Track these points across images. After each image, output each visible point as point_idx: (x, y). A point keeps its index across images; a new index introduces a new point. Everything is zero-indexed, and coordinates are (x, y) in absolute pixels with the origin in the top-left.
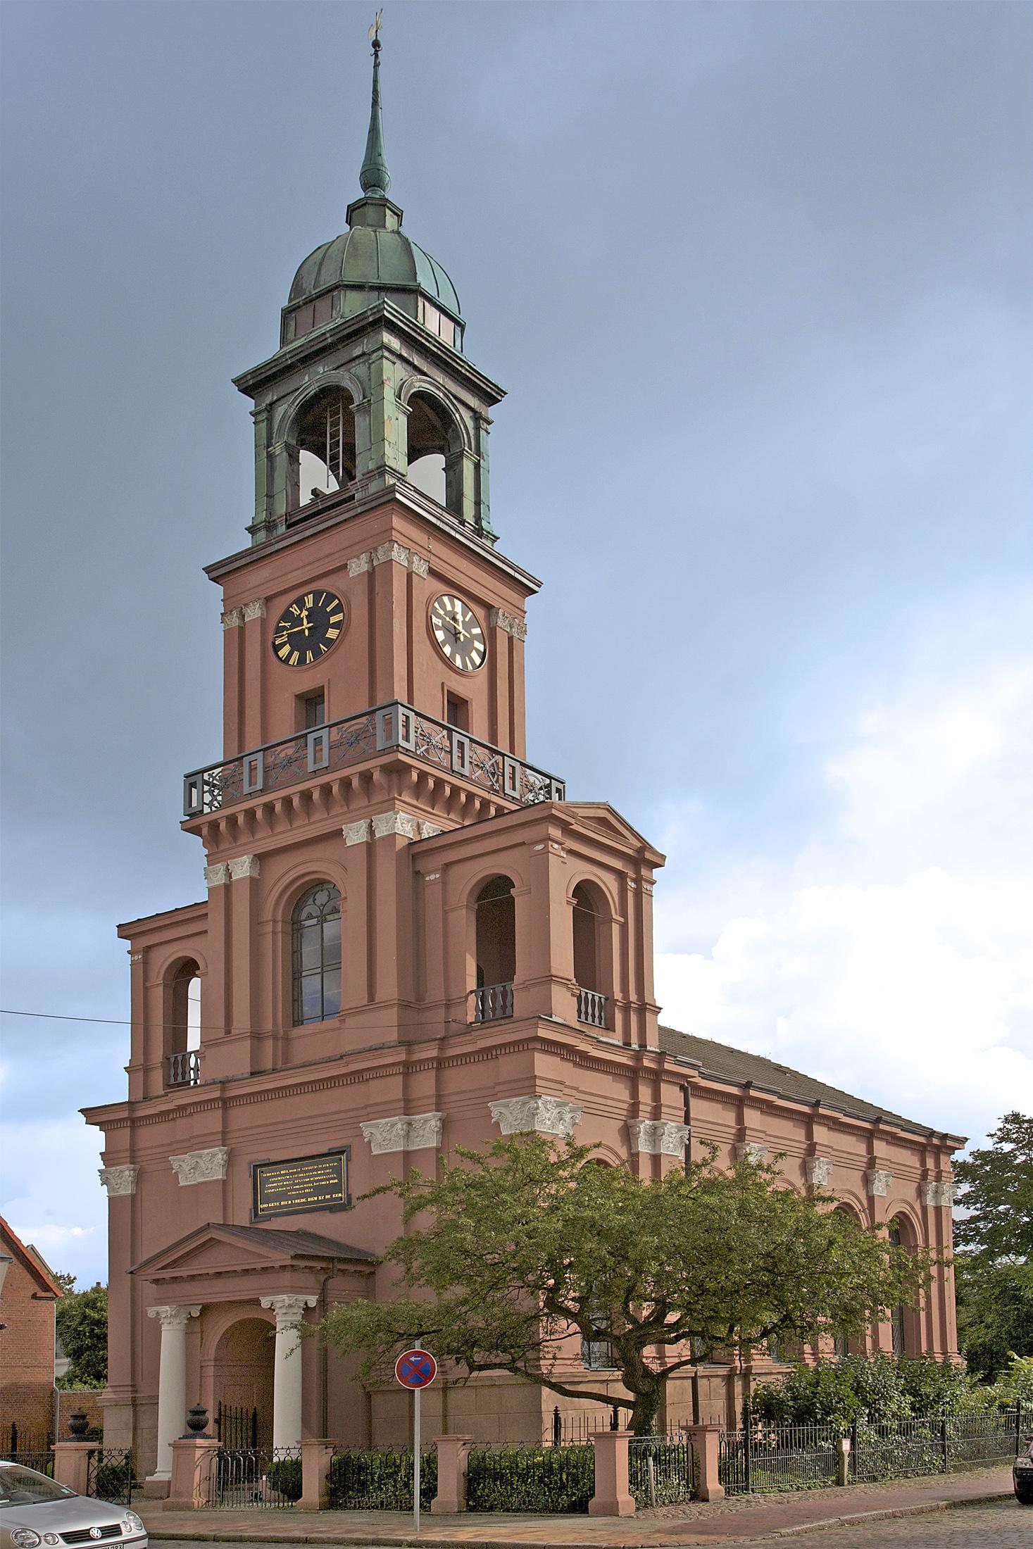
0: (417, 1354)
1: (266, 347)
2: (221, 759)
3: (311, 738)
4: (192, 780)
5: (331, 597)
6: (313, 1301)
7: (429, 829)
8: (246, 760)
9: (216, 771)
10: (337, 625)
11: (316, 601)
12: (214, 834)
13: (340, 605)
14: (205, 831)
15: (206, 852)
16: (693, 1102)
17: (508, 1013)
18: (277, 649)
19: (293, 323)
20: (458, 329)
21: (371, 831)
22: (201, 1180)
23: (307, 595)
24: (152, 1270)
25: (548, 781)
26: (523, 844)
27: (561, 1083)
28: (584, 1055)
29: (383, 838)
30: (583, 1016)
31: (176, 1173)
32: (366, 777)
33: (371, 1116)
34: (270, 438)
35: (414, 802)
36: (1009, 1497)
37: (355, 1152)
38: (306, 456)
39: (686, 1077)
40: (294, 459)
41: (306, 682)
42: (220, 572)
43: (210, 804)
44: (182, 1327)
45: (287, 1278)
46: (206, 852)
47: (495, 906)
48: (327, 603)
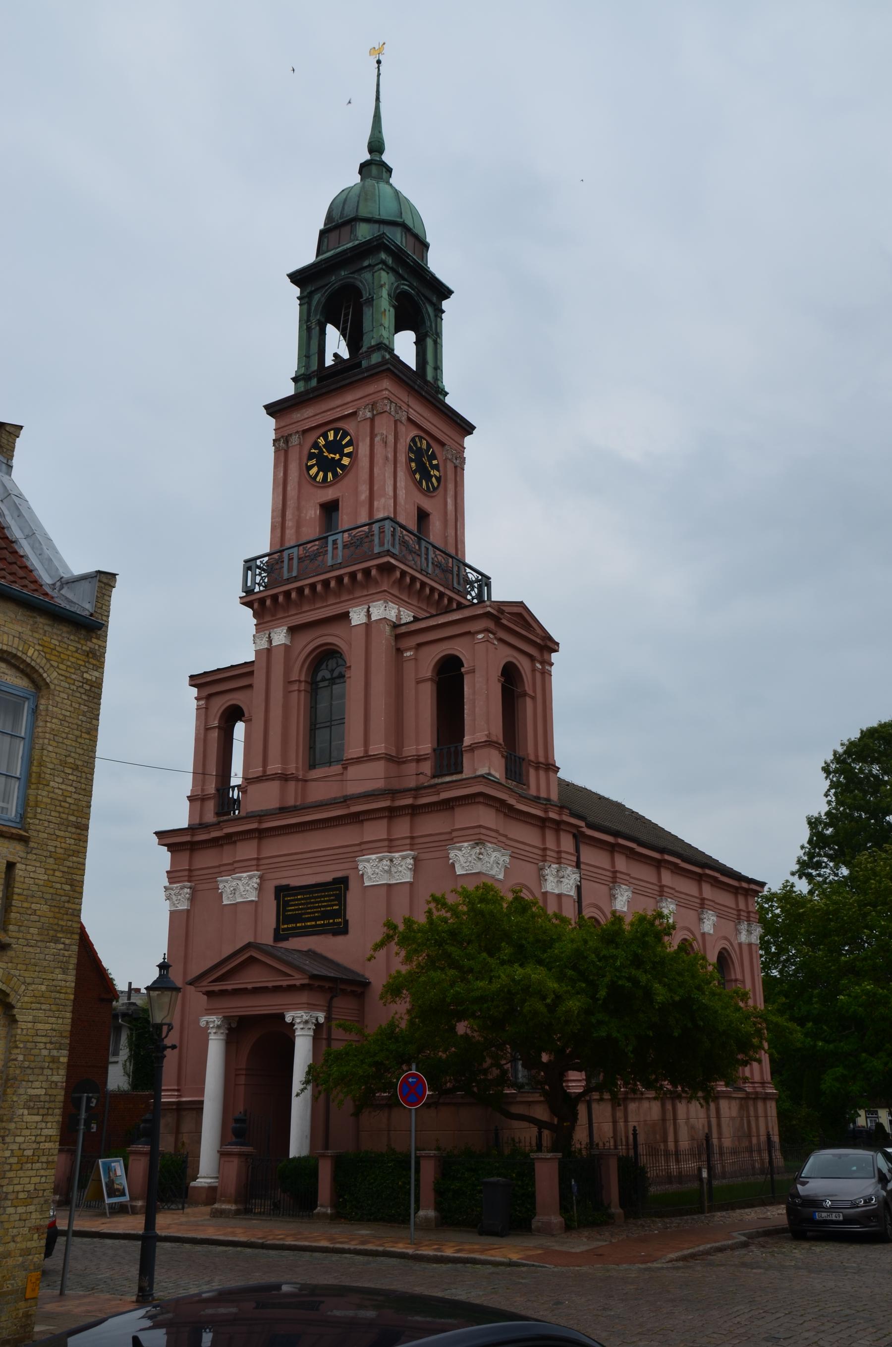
0: (413, 1076)
1: (307, 256)
3: (331, 539)
4: (249, 564)
5: (346, 434)
8: (286, 554)
10: (349, 455)
11: (335, 436)
12: (262, 606)
13: (351, 440)
14: (256, 605)
15: (255, 621)
18: (309, 468)
19: (326, 240)
21: (369, 615)
23: (330, 430)
24: (205, 983)
26: (469, 633)
28: (511, 807)
31: (222, 893)
32: (367, 572)
33: (364, 852)
35: (398, 595)
36: (783, 1231)
37: (352, 884)
41: (329, 495)
42: (273, 409)
43: (259, 584)
45: (304, 998)
47: (449, 678)
48: (343, 438)
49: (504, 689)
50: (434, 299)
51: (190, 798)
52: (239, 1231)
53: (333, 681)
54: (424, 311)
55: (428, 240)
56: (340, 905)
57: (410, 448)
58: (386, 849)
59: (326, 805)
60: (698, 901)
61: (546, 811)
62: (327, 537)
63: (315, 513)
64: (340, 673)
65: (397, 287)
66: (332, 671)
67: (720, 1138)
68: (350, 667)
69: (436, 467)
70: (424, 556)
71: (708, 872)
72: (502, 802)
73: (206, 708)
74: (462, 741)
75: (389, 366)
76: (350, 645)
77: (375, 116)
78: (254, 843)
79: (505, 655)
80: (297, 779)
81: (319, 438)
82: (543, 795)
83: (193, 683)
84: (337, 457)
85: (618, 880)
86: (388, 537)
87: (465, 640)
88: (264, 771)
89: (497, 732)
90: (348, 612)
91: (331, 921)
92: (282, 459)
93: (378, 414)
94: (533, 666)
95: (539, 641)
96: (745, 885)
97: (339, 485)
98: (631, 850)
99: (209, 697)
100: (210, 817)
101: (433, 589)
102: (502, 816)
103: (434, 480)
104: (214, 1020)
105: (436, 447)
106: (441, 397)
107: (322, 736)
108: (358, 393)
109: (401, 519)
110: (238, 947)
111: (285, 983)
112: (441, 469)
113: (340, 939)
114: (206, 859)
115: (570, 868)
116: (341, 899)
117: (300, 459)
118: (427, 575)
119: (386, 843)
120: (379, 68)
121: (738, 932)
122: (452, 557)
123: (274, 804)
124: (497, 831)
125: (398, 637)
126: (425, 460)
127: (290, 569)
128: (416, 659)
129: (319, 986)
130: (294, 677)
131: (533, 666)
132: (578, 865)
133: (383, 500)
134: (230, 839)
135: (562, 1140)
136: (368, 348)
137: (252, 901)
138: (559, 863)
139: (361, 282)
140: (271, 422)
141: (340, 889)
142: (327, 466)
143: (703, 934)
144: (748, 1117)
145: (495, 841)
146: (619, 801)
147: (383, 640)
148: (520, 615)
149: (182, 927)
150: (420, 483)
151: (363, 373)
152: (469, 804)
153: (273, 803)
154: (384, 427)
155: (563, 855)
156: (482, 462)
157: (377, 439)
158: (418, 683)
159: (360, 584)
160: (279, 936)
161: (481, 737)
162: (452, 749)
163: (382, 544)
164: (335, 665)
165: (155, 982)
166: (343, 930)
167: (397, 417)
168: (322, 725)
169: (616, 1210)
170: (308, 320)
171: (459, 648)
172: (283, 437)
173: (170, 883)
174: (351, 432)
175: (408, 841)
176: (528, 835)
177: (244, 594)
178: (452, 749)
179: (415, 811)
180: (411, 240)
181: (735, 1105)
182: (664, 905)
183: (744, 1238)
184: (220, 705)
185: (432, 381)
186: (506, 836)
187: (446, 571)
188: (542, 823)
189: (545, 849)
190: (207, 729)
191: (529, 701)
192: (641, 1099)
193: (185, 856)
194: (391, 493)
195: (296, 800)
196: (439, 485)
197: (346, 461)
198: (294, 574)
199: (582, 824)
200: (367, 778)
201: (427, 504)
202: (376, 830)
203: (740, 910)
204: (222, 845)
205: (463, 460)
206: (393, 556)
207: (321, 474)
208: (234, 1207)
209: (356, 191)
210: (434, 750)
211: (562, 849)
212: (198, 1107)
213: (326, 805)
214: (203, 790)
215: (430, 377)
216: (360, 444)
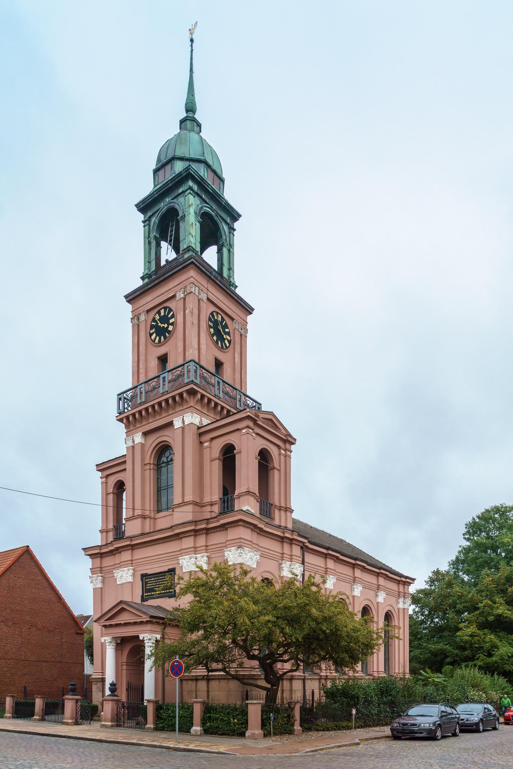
0: (177, 661)
2: (131, 386)
4: (120, 396)
6: (159, 637)
7: (205, 422)
9: (128, 393)
10: (172, 324)
12: (129, 421)
14: (125, 421)
15: (125, 431)
18: (151, 335)
19: (157, 177)
22: (124, 581)
23: (161, 309)
24: (102, 621)
25: (255, 404)
26: (238, 430)
27: (251, 541)
28: (261, 529)
29: (187, 425)
30: (262, 512)
32: (181, 395)
33: (183, 555)
39: (303, 543)
40: (158, 245)
41: (161, 351)
45: (148, 627)
46: (125, 431)
47: (229, 457)
48: (169, 313)
50: (228, 221)
51: (101, 531)
55: (224, 176)
57: (210, 319)
58: (193, 552)
59: (163, 530)
60: (376, 586)
61: (284, 533)
63: (155, 363)
65: (202, 208)
66: (168, 457)
69: (228, 334)
71: (382, 571)
72: (255, 526)
73: (106, 483)
75: (193, 260)
76: (174, 440)
77: (189, 83)
79: (261, 444)
80: (150, 518)
81: (155, 315)
82: (283, 524)
84: (166, 326)
85: (328, 573)
86: (192, 373)
87: (236, 434)
92: (136, 331)
93: (187, 294)
94: (280, 452)
95: (283, 437)
96: (403, 579)
98: (337, 558)
99: (107, 476)
103: (226, 341)
104: (108, 639)
105: (227, 320)
106: (233, 289)
109: (203, 363)
111: (138, 621)
112: (231, 335)
114: (108, 561)
118: (219, 398)
119: (193, 549)
120: (192, 46)
121: (398, 603)
123: (139, 532)
124: (251, 541)
125: (200, 435)
126: (220, 327)
127: (141, 398)
128: (210, 447)
129: (156, 622)
130: (147, 461)
132: (303, 563)
134: (117, 551)
137: (130, 582)
139: (178, 204)
140: (129, 307)
142: (162, 332)
143: (378, 603)
145: (250, 547)
146: (343, 539)
148: (271, 420)
149: (99, 595)
150: (217, 342)
153: (138, 531)
154: (191, 304)
158: (211, 461)
159: (175, 403)
160: (143, 599)
161: (244, 489)
162: (230, 498)
163: (189, 377)
164: (169, 454)
170: (149, 237)
171: (232, 439)
174: (173, 308)
175: (204, 548)
176: (274, 546)
179: (208, 531)
180: (211, 174)
182: (355, 587)
183: (358, 741)
184: (112, 480)
185: (227, 278)
188: (282, 539)
189: (283, 554)
190: (107, 494)
191: (276, 472)
193: (98, 560)
194: (196, 346)
196: (229, 346)
197: (171, 328)
198: (143, 400)
199: (306, 541)
200: (183, 515)
201: (221, 357)
202: (188, 542)
203: (400, 592)
204: (115, 554)
205: (246, 331)
206: (196, 384)
207: (158, 338)
208: (110, 724)
210: (220, 499)
211: (293, 554)
213: (163, 530)
214: (107, 527)
215: (225, 274)
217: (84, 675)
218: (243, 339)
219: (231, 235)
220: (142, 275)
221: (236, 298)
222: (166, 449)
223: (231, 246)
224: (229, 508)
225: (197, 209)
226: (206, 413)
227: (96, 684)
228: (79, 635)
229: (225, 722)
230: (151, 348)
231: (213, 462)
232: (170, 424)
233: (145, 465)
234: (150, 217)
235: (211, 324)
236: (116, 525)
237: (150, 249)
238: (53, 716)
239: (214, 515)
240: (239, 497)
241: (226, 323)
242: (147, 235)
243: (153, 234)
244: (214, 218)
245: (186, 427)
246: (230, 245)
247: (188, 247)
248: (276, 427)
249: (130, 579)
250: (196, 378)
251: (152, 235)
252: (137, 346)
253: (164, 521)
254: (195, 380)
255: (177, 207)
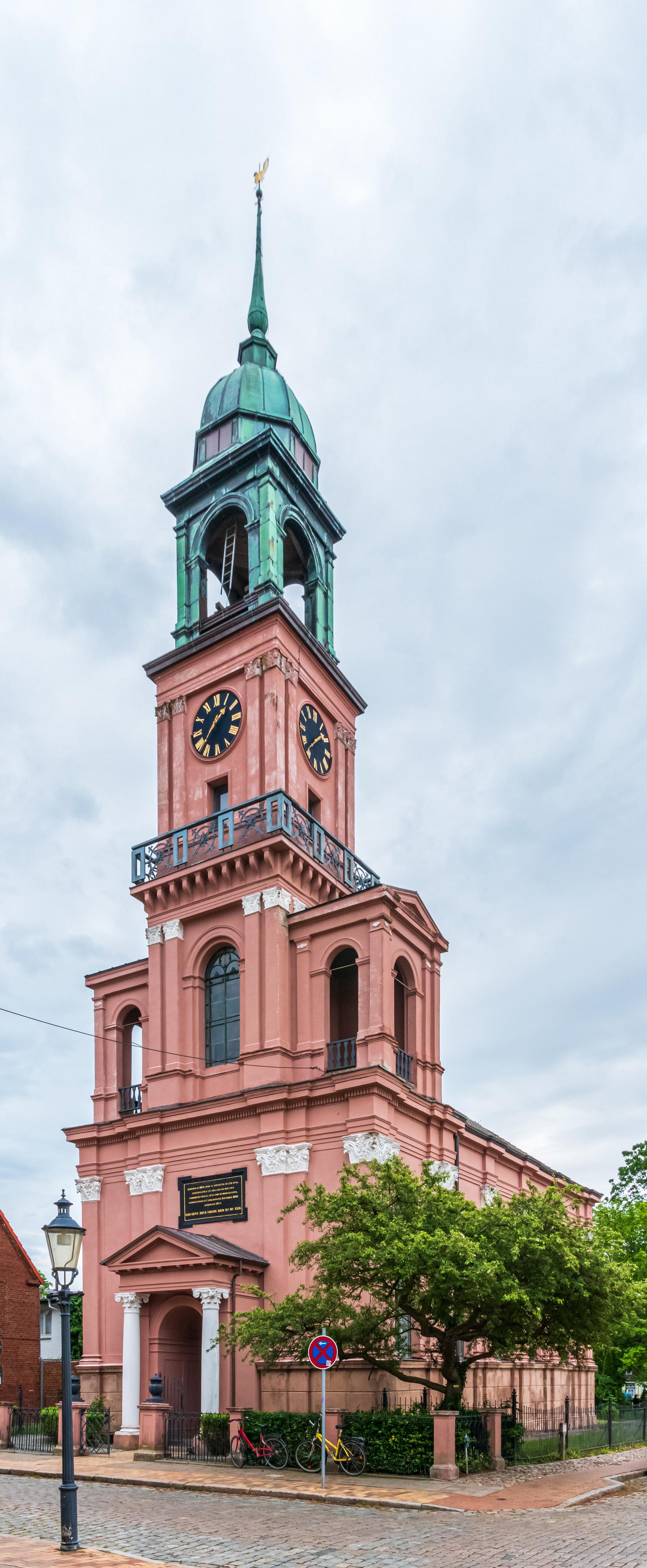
1: (181, 470)
2: (155, 835)
3: (220, 818)
4: (137, 851)
7: (300, 905)
11: (222, 701)
12: (155, 898)
13: (239, 705)
14: (147, 897)
15: (147, 915)
16: (462, 1150)
17: (352, 1064)
18: (195, 741)
19: (203, 446)
20: (315, 468)
22: (145, 1191)
23: (215, 694)
24: (117, 1263)
25: (369, 876)
26: (365, 922)
28: (401, 1102)
31: (128, 1185)
32: (259, 854)
33: (262, 1144)
34: (187, 552)
37: (251, 1174)
38: (210, 574)
40: (203, 576)
41: (217, 770)
44: (137, 1311)
45: (211, 1275)
46: (147, 915)
47: (343, 972)
48: (230, 702)
49: (397, 985)
50: (325, 538)
52: (161, 1473)
53: (226, 977)
54: (314, 551)
55: (319, 454)
56: (239, 1194)
61: (432, 1110)
62: (216, 818)
63: (203, 793)
64: (234, 968)
65: (286, 511)
66: (226, 967)
67: (552, 1401)
68: (244, 960)
70: (316, 846)
72: (394, 1094)
74: (356, 1036)
76: (243, 937)
78: (157, 1137)
81: (204, 704)
83: (90, 983)
85: (488, 1181)
87: (361, 929)
88: (163, 1068)
89: (390, 1029)
90: (241, 901)
91: (231, 1209)
94: (424, 964)
95: (430, 938)
97: (226, 760)
99: (106, 998)
100: (114, 1115)
101: (325, 880)
102: (393, 1109)
104: (130, 1296)
107: (218, 1034)
108: (246, 645)
110: (146, 1229)
111: (191, 1263)
113: (240, 1225)
114: (111, 1154)
115: (450, 1166)
116: (240, 1189)
117: (186, 731)
119: (283, 1135)
122: (343, 849)
124: (389, 1123)
125: (292, 928)
127: (180, 856)
130: (188, 973)
131: (424, 964)
132: (456, 1163)
133: (274, 773)
134: (134, 1135)
135: (452, 1401)
136: (255, 589)
137: (157, 1192)
138: (441, 1160)
139: (245, 501)
140: (152, 688)
141: (239, 1180)
144: (573, 1385)
145: (386, 1132)
147: (277, 930)
148: (413, 906)
151: (250, 617)
152: (363, 1095)
153: (171, 1100)
154: (275, 685)
155: (445, 1153)
156: (376, 742)
157: (267, 701)
158: (312, 976)
159: (251, 866)
160: (183, 1224)
161: (375, 1030)
162: (346, 1044)
163: (275, 822)
164: (228, 961)
165: (53, 1222)
166: (243, 1217)
167: (288, 676)
168: (217, 1023)
169: (499, 1459)
170: (187, 558)
171: (353, 938)
172: (165, 704)
173: (81, 1177)
174: (239, 694)
177: (134, 885)
178: (346, 1044)
179: (310, 1103)
181: (565, 1375)
184: (117, 1005)
186: (396, 1129)
187: (337, 864)
189: (429, 1146)
191: (418, 1000)
192: (497, 1369)
193: (92, 1152)
194: (283, 767)
195: (195, 1097)
198: (184, 860)
200: (258, 1074)
201: (320, 789)
202: (273, 1122)
204: (126, 1141)
205: (354, 745)
206: (287, 836)
209: (237, 376)
210: (328, 1045)
212: (117, 1371)
213: (224, 1098)
216: (249, 708)
217: (39, 1362)
218: (349, 758)
219: (329, 566)
220: (174, 629)
221: (342, 683)
222: (222, 952)
223: (328, 585)
224: (346, 1062)
225: (279, 512)
226: (299, 889)
227: (89, 1378)
228: (31, 1288)
229: (388, 1448)
230: (196, 766)
231: (314, 979)
232: (237, 906)
233: (184, 979)
234: (189, 521)
235: (303, 728)
236: (121, 1087)
237: (189, 581)
238: (25, 1438)
239: (317, 1074)
240: (366, 1042)
241: (324, 727)
242: (183, 554)
243: (197, 553)
244: (303, 533)
245: (267, 914)
246: (328, 585)
247: (266, 583)
248: (420, 919)
249: (158, 1187)
250: (287, 825)
251: (193, 556)
252: (167, 761)
253: (221, 1083)
254: (285, 829)
255: (242, 505)
